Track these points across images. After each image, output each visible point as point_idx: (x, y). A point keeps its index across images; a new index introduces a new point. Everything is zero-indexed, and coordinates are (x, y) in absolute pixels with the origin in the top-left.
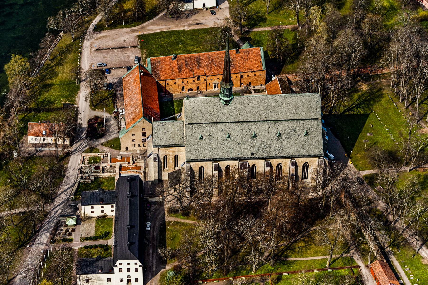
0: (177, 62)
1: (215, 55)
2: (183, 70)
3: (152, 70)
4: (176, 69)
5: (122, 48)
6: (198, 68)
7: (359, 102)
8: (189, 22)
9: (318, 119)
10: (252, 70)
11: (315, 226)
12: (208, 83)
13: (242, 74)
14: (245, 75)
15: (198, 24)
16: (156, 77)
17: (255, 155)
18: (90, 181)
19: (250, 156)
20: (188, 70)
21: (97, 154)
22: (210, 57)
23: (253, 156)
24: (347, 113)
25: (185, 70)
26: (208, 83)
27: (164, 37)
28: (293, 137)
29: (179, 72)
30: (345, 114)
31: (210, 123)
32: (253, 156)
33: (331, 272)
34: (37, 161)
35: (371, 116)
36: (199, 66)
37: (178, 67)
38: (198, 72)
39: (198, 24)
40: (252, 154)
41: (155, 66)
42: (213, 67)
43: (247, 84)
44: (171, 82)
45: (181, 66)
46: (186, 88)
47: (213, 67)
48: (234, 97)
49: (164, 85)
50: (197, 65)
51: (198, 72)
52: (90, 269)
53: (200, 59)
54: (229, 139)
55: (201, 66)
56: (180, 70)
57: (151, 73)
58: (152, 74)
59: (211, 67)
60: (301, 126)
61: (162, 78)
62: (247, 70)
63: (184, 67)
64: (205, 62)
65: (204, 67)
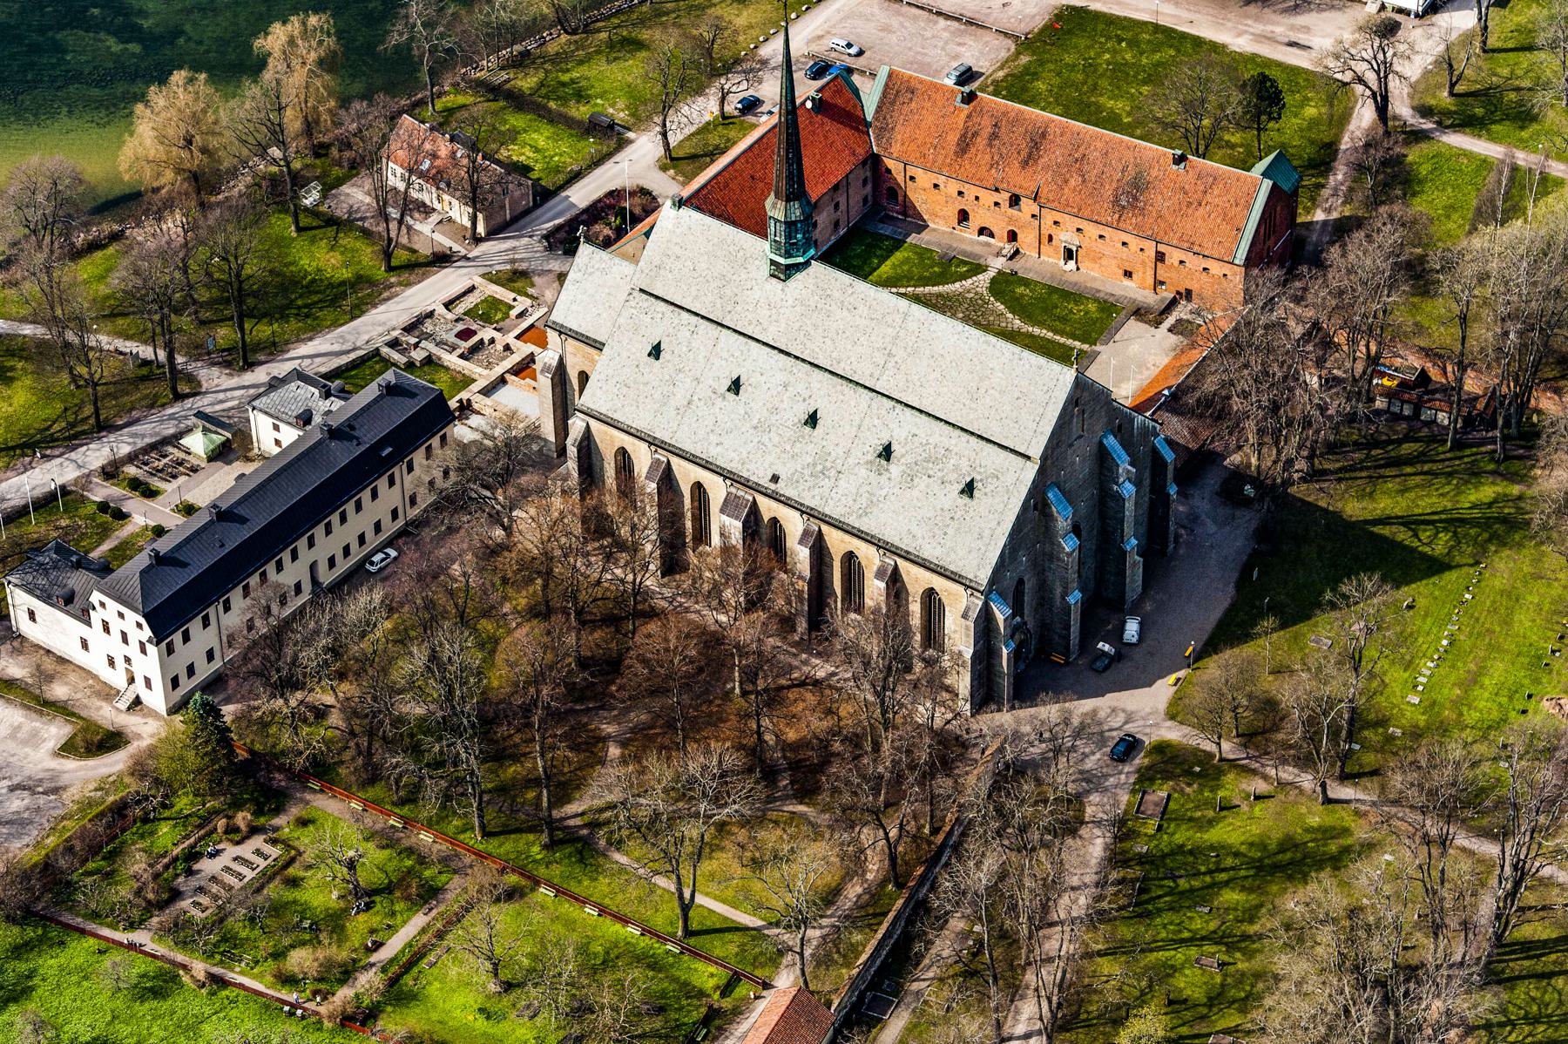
0: (969, 116)
1: (1099, 145)
2: (973, 150)
3: (879, 109)
4: (953, 138)
5: (970, 23)
6: (1025, 164)
7: (1476, 513)
8: (1270, 28)
9: (1028, 458)
10: (1196, 249)
11: (808, 805)
12: (1045, 233)
13: (1162, 248)
14: (1174, 256)
15: (1292, 44)
16: (878, 138)
17: (781, 483)
18: (404, 360)
19: (765, 482)
20: (988, 157)
21: (513, 295)
22: (1078, 142)
23: (773, 486)
24: (1385, 531)
25: (981, 151)
26: (1045, 233)
27: (1134, 43)
28: (922, 482)
29: (956, 153)
30: (1376, 529)
31: (703, 317)
32: (773, 486)
33: (674, 956)
34: (536, 279)
35: (1451, 576)
36: (1029, 157)
37: (964, 136)
38: (1023, 182)
39: (1292, 44)
40: (775, 479)
41: (893, 103)
42: (1072, 182)
43: (1178, 293)
44: (924, 179)
45: (975, 134)
46: (975, 222)
47: (1074, 181)
48: (807, 264)
49: (900, 179)
50: (1024, 154)
51: (1023, 182)
52: (42, 581)
53: (1043, 135)
54: (731, 396)
55: (1036, 161)
56: (964, 146)
57: (869, 118)
58: (868, 125)
59: (1066, 181)
60: (968, 456)
61: (896, 149)
62: (1181, 239)
63: (981, 142)
64: (1053, 155)
65: (1046, 168)
